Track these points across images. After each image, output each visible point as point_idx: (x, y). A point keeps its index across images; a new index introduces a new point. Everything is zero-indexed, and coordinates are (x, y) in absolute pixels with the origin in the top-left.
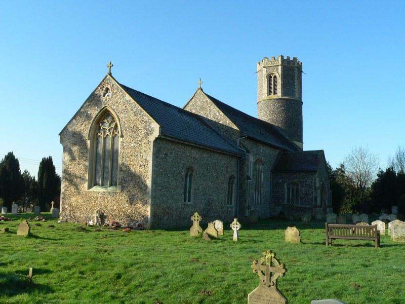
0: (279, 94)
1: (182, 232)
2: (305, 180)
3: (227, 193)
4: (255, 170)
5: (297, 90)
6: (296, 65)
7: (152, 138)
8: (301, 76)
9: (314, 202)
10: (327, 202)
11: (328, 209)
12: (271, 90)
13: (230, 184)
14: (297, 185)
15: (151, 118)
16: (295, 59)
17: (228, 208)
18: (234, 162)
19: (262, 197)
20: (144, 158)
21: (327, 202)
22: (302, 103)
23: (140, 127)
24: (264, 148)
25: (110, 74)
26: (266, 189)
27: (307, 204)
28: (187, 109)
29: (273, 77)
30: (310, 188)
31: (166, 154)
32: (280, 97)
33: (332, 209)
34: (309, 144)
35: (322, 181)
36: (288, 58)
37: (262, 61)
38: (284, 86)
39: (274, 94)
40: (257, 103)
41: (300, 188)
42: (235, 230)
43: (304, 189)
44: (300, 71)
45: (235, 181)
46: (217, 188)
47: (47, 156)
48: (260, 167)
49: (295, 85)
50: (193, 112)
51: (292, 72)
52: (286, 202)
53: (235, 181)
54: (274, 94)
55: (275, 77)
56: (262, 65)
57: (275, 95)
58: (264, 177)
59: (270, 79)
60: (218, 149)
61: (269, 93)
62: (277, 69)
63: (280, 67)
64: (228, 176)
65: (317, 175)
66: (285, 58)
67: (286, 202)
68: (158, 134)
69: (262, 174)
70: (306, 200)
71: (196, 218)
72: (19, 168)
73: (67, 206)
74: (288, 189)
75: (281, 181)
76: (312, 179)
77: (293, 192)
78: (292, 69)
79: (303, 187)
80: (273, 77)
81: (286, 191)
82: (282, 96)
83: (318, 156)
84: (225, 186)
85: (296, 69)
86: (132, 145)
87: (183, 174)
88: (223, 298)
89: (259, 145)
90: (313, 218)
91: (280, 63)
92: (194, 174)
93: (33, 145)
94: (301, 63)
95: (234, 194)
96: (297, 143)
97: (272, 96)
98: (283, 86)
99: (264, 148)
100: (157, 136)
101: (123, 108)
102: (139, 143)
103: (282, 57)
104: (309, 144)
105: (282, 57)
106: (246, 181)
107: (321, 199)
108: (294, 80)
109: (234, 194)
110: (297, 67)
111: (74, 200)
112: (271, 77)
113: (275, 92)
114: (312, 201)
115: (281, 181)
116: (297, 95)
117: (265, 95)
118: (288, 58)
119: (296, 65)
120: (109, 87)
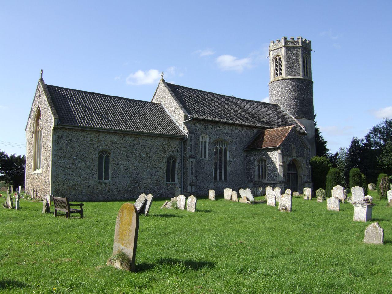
0: (284, 75)
1: (214, 197)
3: (165, 171)
12: (278, 71)
22: (312, 82)
27: (272, 180)
28: (153, 101)
29: (278, 58)
32: (284, 78)
43: (270, 165)
51: (300, 54)
55: (280, 58)
57: (281, 76)
58: (231, 156)
59: (277, 60)
61: (276, 75)
62: (281, 51)
64: (166, 156)
66: (289, 39)
69: (228, 153)
70: (271, 176)
72: (313, 113)
74: (259, 166)
75: (252, 158)
77: (262, 169)
80: (278, 58)
81: (257, 167)
82: (286, 76)
88: (7, 250)
94: (310, 42)
98: (287, 67)
103: (285, 39)
105: (285, 39)
108: (298, 60)
111: (160, 165)
112: (277, 60)
113: (281, 74)
115: (252, 158)
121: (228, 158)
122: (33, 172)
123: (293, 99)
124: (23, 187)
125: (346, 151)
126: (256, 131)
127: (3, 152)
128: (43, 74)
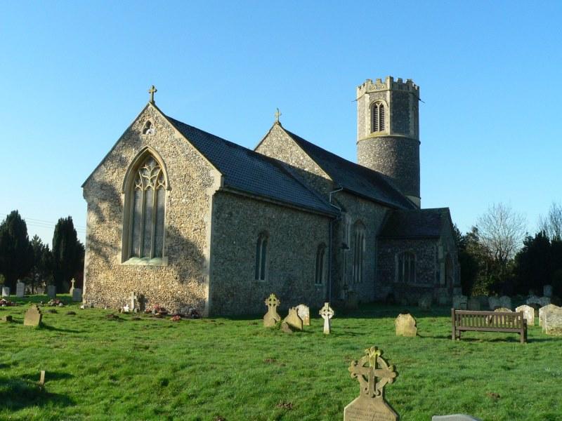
0: (387, 130)
2: (423, 249)
3: (315, 267)
4: (354, 235)
5: (412, 124)
6: (411, 90)
7: (211, 191)
8: (418, 105)
9: (436, 280)
10: (454, 280)
11: (455, 290)
12: (376, 125)
13: (320, 254)
14: (413, 256)
15: (209, 163)
16: (409, 82)
17: (316, 288)
18: (324, 224)
19: (364, 272)
20: (200, 219)
21: (454, 280)
22: (420, 143)
23: (194, 176)
24: (367, 205)
25: (153, 103)
26: (369, 262)
27: (425, 283)
29: (378, 106)
30: (431, 260)
31: (231, 214)
32: (389, 135)
33: (460, 289)
34: (429, 200)
35: (447, 251)
36: (400, 80)
37: (364, 85)
38: (394, 119)
39: (381, 130)
40: (357, 143)
41: (416, 260)
42: (326, 319)
43: (421, 262)
44: (417, 98)
45: (327, 250)
46: (301, 260)
47: (65, 217)
48: (361, 231)
49: (409, 118)
50: (268, 155)
51: (405, 100)
52: (396, 280)
53: (327, 250)
54: (381, 130)
55: (382, 106)
56: (364, 90)
57: (382, 132)
58: (367, 245)
59: (375, 109)
60: (303, 206)
61: (374, 129)
62: (385, 96)
63: (388, 93)
64: (316, 243)
65: (440, 242)
66: (396, 80)
67: (396, 280)
68: (220, 186)
69: (364, 241)
70: (424, 277)
71: (272, 303)
73: (92, 286)
74: (400, 262)
75: (389, 250)
76: (433, 248)
77: (406, 265)
78: (406, 96)
79: (420, 258)
80: (378, 106)
81: (397, 264)
82: (391, 133)
83: (441, 217)
84: (313, 257)
85: (411, 95)
86: (184, 200)
87: (254, 241)
89: (360, 200)
90: (435, 302)
91: (389, 87)
92: (269, 241)
93: (46, 201)
94: (418, 88)
95: (325, 269)
96: (412, 198)
97: (378, 133)
98: (393, 119)
99: (367, 205)
100: (218, 189)
101: (171, 149)
102: (192, 198)
103: (392, 79)
104: (429, 200)
105: (392, 79)
106: (341, 250)
107: (446, 276)
108: (407, 111)
109: (325, 269)
110: (413, 93)
112: (376, 107)
113: (382, 128)
114: (433, 278)
115: (389, 250)
116: (412, 132)
117: (367, 132)
118: (400, 80)
119: (411, 90)
120: (151, 120)
121: (364, 250)
122: (122, 262)
123: (401, 166)
124: (79, 285)
125: (520, 246)
126: (385, 209)
127: (525, 243)
128: (156, 104)
